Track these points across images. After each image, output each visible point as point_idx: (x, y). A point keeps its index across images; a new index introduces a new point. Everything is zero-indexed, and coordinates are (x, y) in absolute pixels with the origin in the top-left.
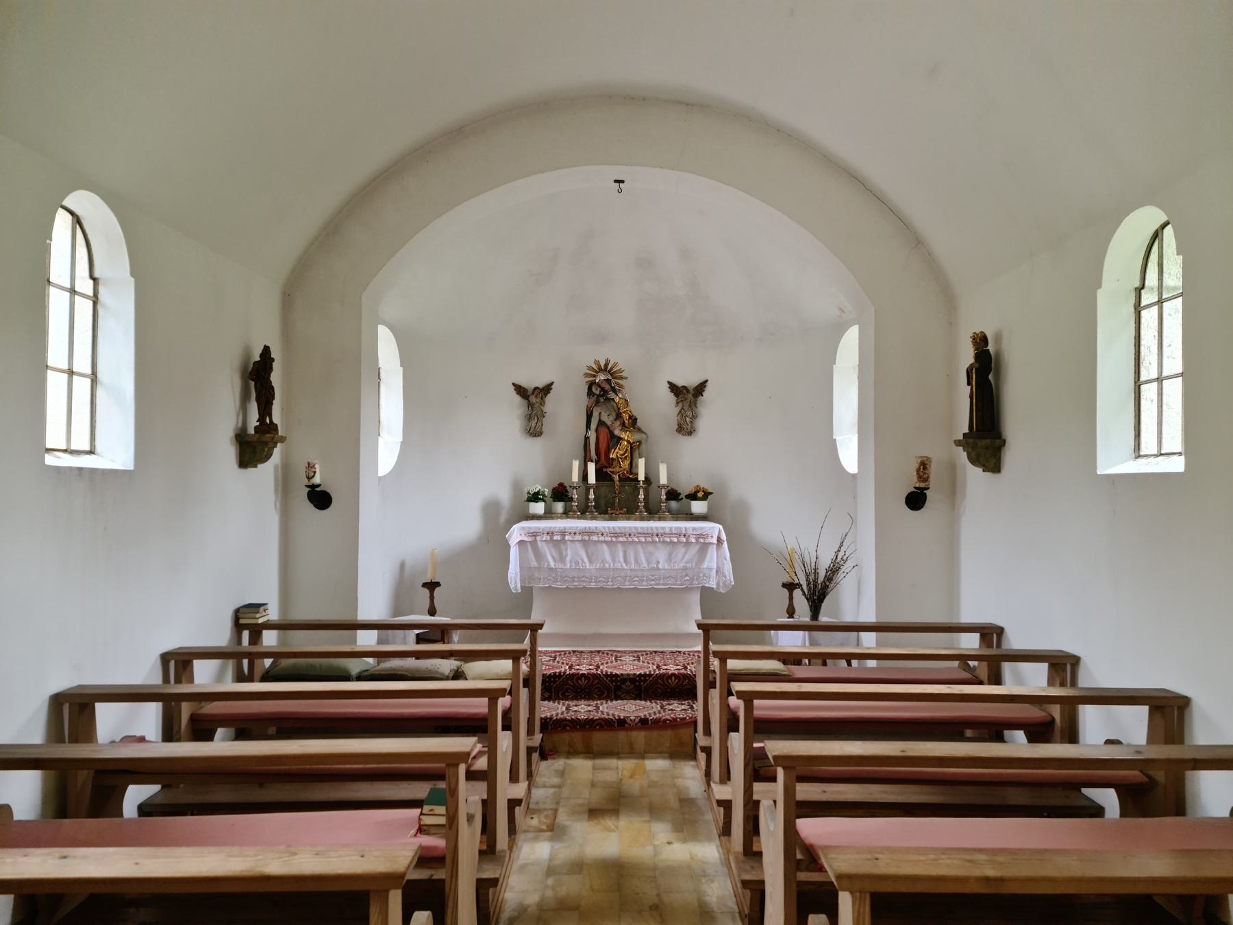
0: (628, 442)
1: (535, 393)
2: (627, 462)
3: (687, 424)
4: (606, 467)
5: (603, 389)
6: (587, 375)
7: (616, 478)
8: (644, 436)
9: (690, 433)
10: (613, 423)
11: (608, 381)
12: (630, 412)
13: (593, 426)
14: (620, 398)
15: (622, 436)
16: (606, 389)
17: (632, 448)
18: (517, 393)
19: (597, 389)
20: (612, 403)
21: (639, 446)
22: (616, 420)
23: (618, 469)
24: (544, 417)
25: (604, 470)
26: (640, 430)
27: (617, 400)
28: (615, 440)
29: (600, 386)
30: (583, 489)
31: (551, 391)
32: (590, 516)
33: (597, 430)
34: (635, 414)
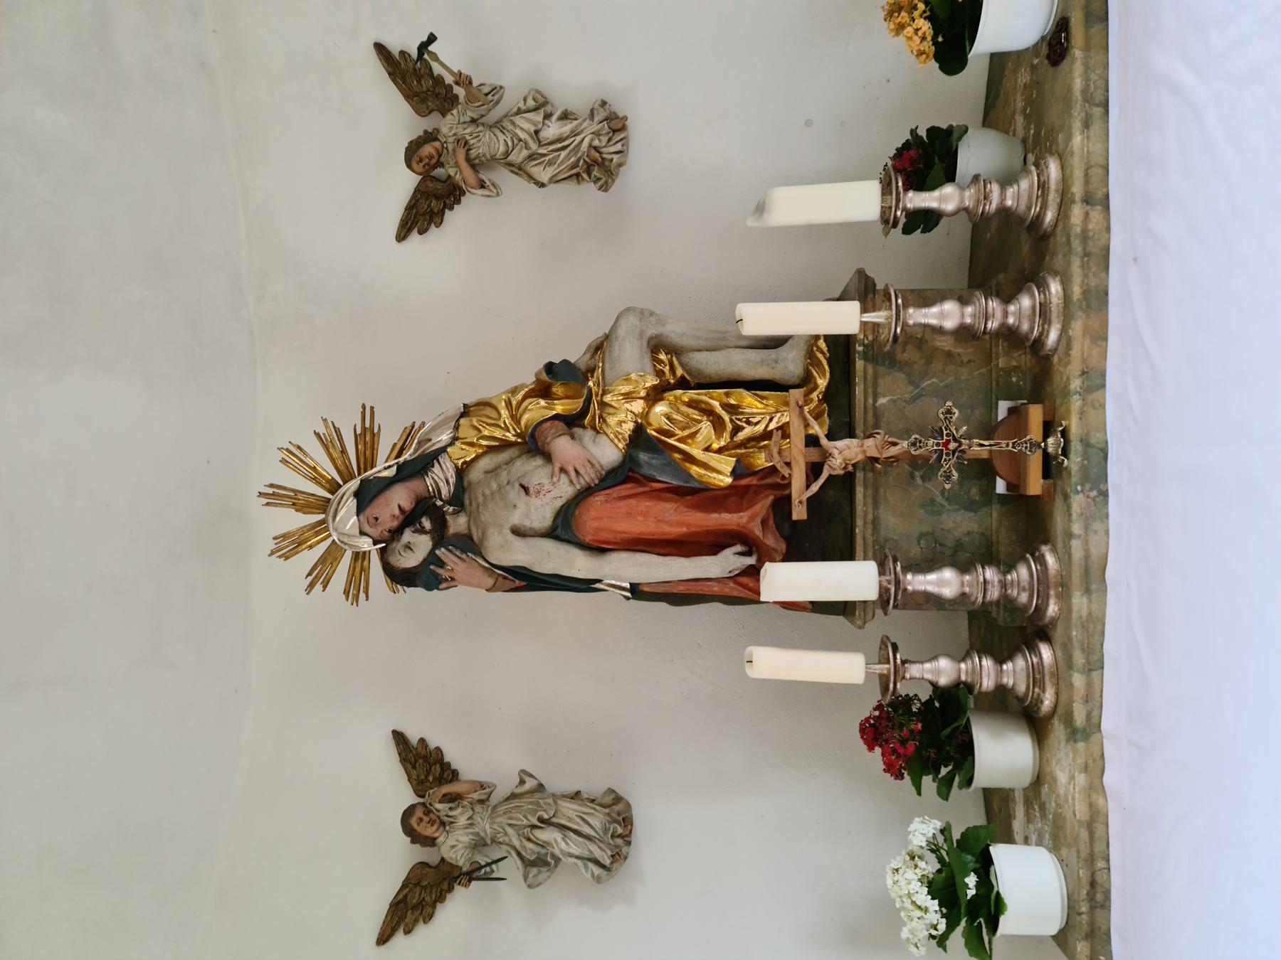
0: (655, 395)
1: (429, 831)
2: (750, 401)
3: (574, 134)
4: (783, 504)
5: (409, 520)
6: (356, 588)
7: (844, 452)
8: (629, 326)
9: (616, 125)
10: (562, 470)
11: (367, 495)
12: (514, 391)
13: (577, 564)
14: (455, 439)
15: (628, 427)
16: (407, 505)
17: (683, 384)
18: (429, 918)
19: (408, 547)
20: (475, 474)
21: (674, 351)
22: (548, 457)
23: (799, 456)
24: (541, 787)
25: (799, 512)
26: (599, 348)
27: (461, 453)
28: (643, 457)
29: (396, 533)
30: (896, 624)
31: (433, 743)
32: (1079, 601)
33: (598, 549)
34: (528, 376)
